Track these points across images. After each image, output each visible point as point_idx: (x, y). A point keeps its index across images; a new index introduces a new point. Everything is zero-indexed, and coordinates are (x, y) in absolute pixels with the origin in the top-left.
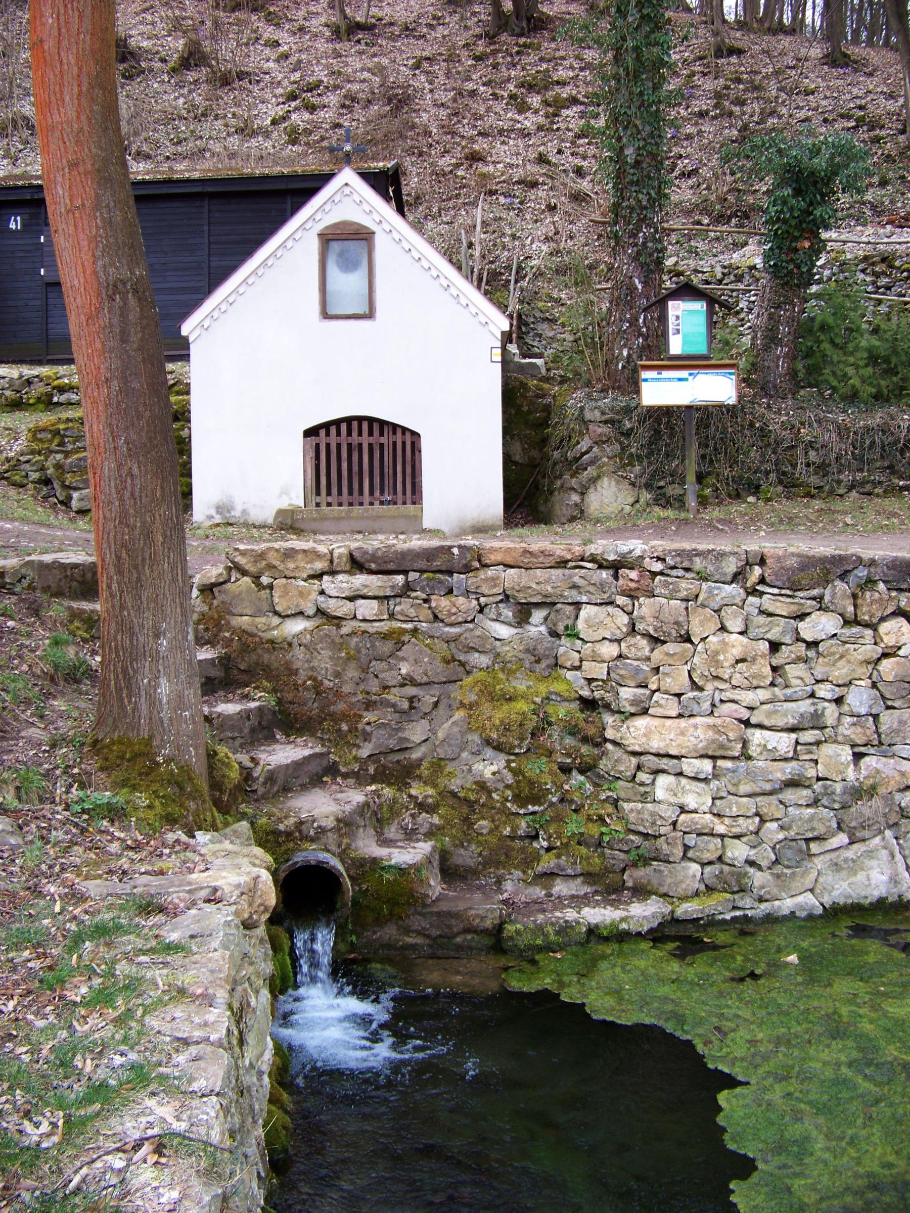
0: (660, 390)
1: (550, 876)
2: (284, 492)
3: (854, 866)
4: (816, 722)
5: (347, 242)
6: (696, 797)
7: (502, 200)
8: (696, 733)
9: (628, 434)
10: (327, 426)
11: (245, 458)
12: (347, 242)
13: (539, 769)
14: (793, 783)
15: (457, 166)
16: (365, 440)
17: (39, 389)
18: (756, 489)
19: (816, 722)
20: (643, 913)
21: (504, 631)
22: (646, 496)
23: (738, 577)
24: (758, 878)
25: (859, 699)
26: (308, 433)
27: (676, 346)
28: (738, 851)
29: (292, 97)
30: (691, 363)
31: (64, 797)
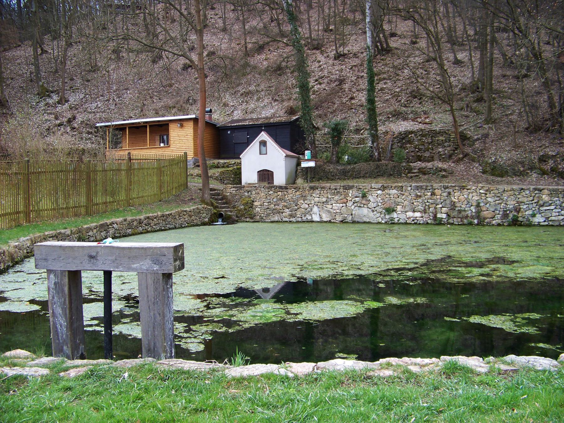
0: (304, 165)
1: (246, 218)
3: (274, 217)
4: (270, 202)
6: (259, 210)
7: (354, 110)
8: (259, 203)
11: (249, 176)
12: (263, 143)
13: (246, 207)
14: (268, 208)
17: (227, 164)
18: (321, 179)
19: (270, 202)
24: (264, 218)
28: (262, 215)
29: (316, 80)
31: (348, 403)
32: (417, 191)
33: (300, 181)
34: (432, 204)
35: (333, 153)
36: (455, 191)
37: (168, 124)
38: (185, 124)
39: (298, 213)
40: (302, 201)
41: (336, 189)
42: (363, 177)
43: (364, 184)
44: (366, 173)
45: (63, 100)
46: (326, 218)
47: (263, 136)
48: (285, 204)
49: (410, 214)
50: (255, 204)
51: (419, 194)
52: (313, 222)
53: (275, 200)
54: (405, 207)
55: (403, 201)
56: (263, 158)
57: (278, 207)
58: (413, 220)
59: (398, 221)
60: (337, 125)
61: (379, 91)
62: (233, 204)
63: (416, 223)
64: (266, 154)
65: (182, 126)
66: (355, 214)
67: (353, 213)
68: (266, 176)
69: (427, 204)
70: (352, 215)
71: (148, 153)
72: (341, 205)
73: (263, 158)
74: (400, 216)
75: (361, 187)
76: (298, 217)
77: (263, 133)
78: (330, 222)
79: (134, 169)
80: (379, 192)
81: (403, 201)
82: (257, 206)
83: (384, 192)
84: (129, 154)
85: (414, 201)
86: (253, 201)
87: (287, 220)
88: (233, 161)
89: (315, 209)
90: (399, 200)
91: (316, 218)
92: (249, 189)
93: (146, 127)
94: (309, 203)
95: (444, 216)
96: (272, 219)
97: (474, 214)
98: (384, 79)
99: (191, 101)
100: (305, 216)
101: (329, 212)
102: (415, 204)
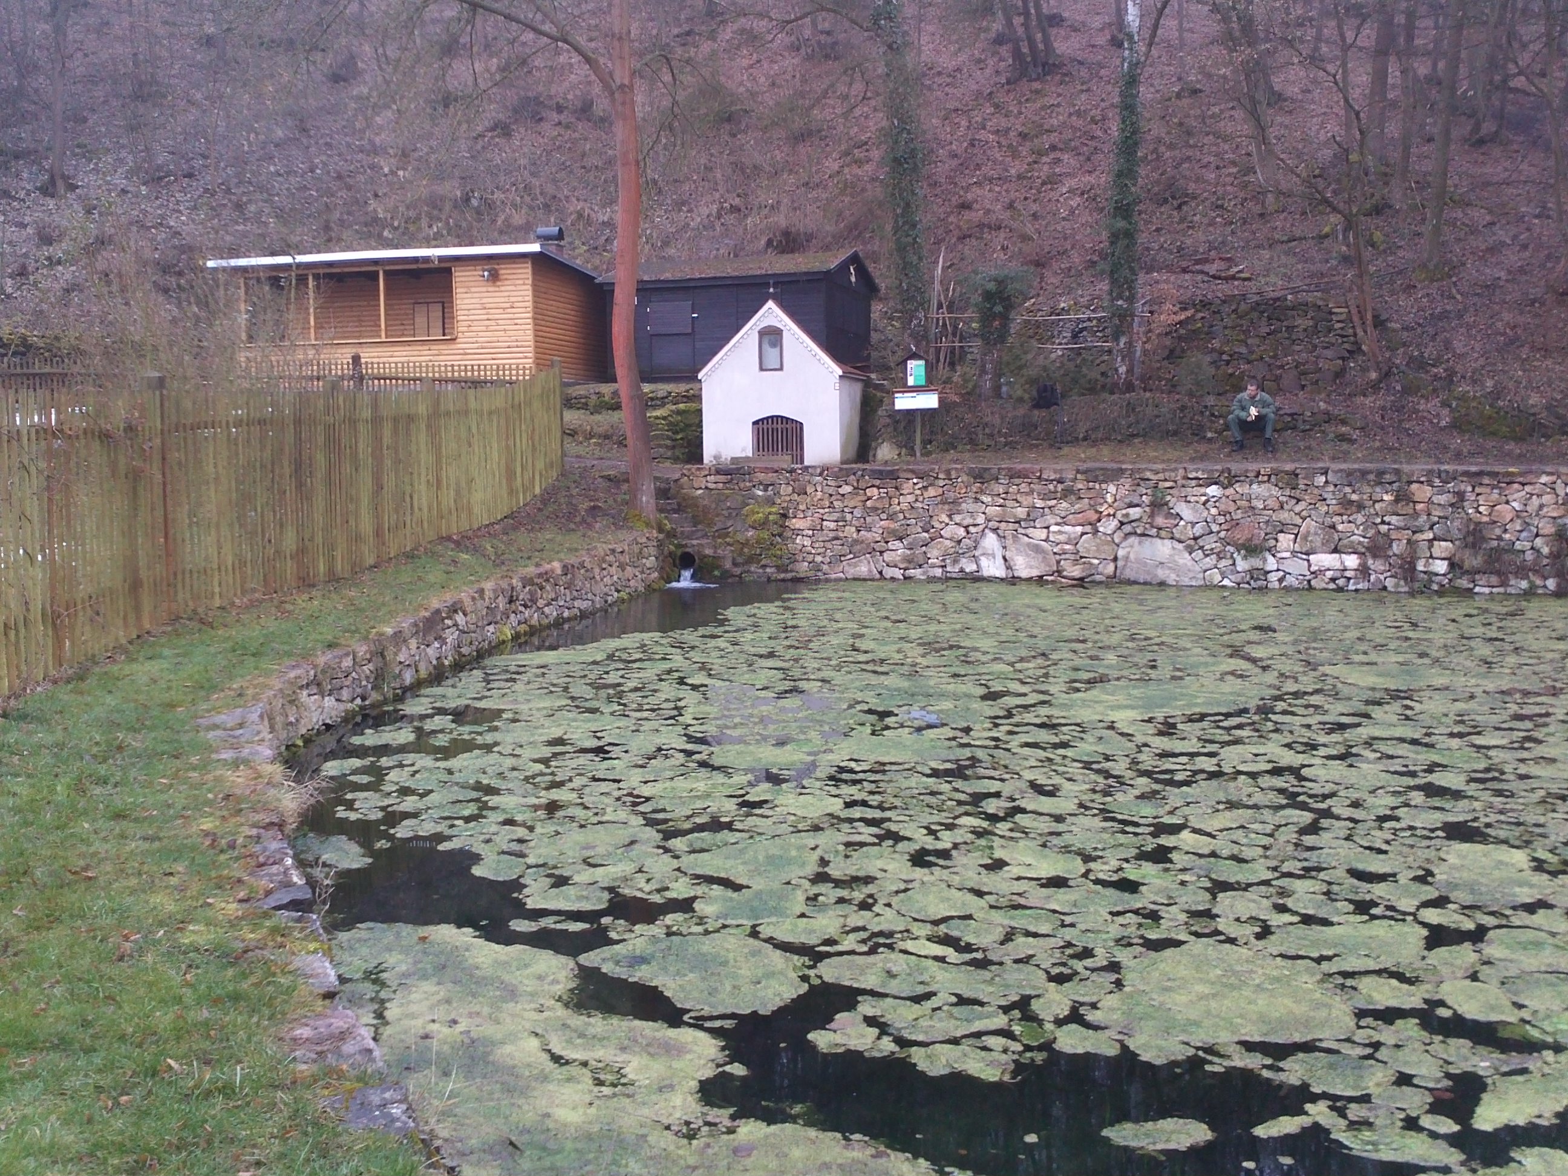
0: (904, 402)
2: (743, 450)
5: (772, 336)
9: (897, 422)
10: (762, 420)
11: (726, 436)
12: (772, 336)
15: (949, 214)
16: (779, 426)
20: (789, 576)
21: (760, 493)
22: (904, 451)
23: (820, 475)
24: (825, 567)
25: (858, 513)
26: (754, 423)
27: (911, 382)
30: (917, 389)
32: (1348, 490)
33: (885, 452)
34: (1398, 528)
35: (984, 366)
36: (1478, 490)
37: (449, 271)
38: (504, 271)
39: (934, 553)
40: (944, 518)
41: (1060, 481)
42: (1085, 439)
43: (1157, 462)
44: (1096, 429)
45: (60, 183)
46: (1024, 567)
47: (772, 314)
48: (893, 525)
49: (1324, 560)
50: (796, 523)
51: (1354, 497)
52: (982, 579)
53: (858, 513)
54: (1305, 539)
55: (1299, 521)
56: (763, 385)
57: (869, 535)
58: (1333, 580)
59: (1281, 580)
60: (1001, 282)
61: (1044, 183)
62: (719, 526)
63: (1340, 589)
64: (781, 369)
65: (494, 277)
66: (1127, 558)
67: (1121, 553)
68: (779, 434)
69: (1384, 528)
70: (1115, 559)
71: (394, 357)
72: (1079, 529)
73: (763, 385)
74: (1288, 566)
75: (1148, 475)
76: (933, 566)
77: (770, 304)
78: (1040, 580)
79: (448, 413)
80: (1213, 490)
81: (1299, 521)
82: (797, 532)
83: (1230, 491)
84: (356, 359)
85: (1337, 519)
86: (784, 516)
87: (898, 574)
88: (681, 388)
89: (990, 541)
90: (1284, 516)
91: (993, 568)
92: (771, 477)
93: (374, 276)
94: (968, 521)
95: (1441, 567)
96: (851, 572)
97: (1545, 561)
98: (1053, 148)
99: (475, 202)
100: (955, 562)
101: (1037, 549)
102: (1340, 527)
